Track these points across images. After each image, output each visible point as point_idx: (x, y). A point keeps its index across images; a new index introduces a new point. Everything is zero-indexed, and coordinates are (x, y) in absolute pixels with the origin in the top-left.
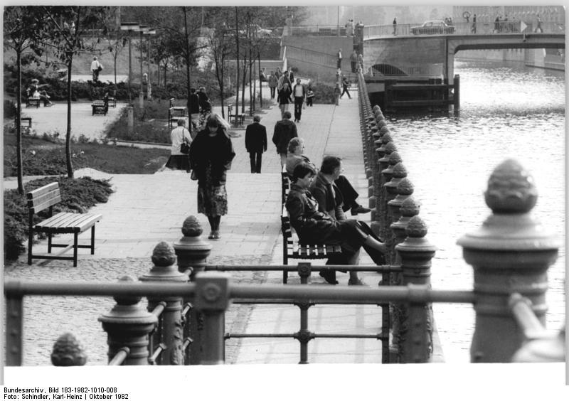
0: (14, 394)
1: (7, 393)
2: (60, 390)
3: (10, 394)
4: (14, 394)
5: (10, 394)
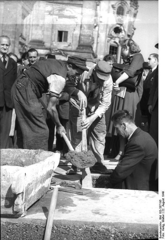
0: (162, 234)
1: (162, 237)
2: (161, 215)
3: (162, 236)
4: (162, 234)
5: (162, 236)
